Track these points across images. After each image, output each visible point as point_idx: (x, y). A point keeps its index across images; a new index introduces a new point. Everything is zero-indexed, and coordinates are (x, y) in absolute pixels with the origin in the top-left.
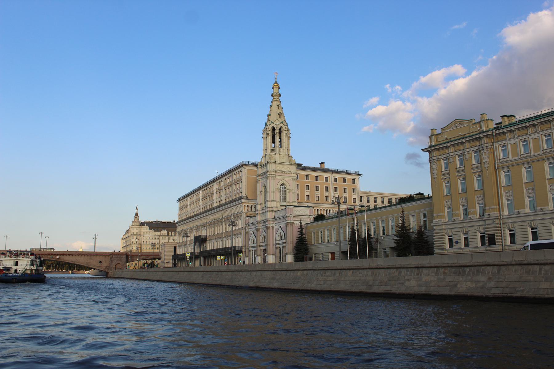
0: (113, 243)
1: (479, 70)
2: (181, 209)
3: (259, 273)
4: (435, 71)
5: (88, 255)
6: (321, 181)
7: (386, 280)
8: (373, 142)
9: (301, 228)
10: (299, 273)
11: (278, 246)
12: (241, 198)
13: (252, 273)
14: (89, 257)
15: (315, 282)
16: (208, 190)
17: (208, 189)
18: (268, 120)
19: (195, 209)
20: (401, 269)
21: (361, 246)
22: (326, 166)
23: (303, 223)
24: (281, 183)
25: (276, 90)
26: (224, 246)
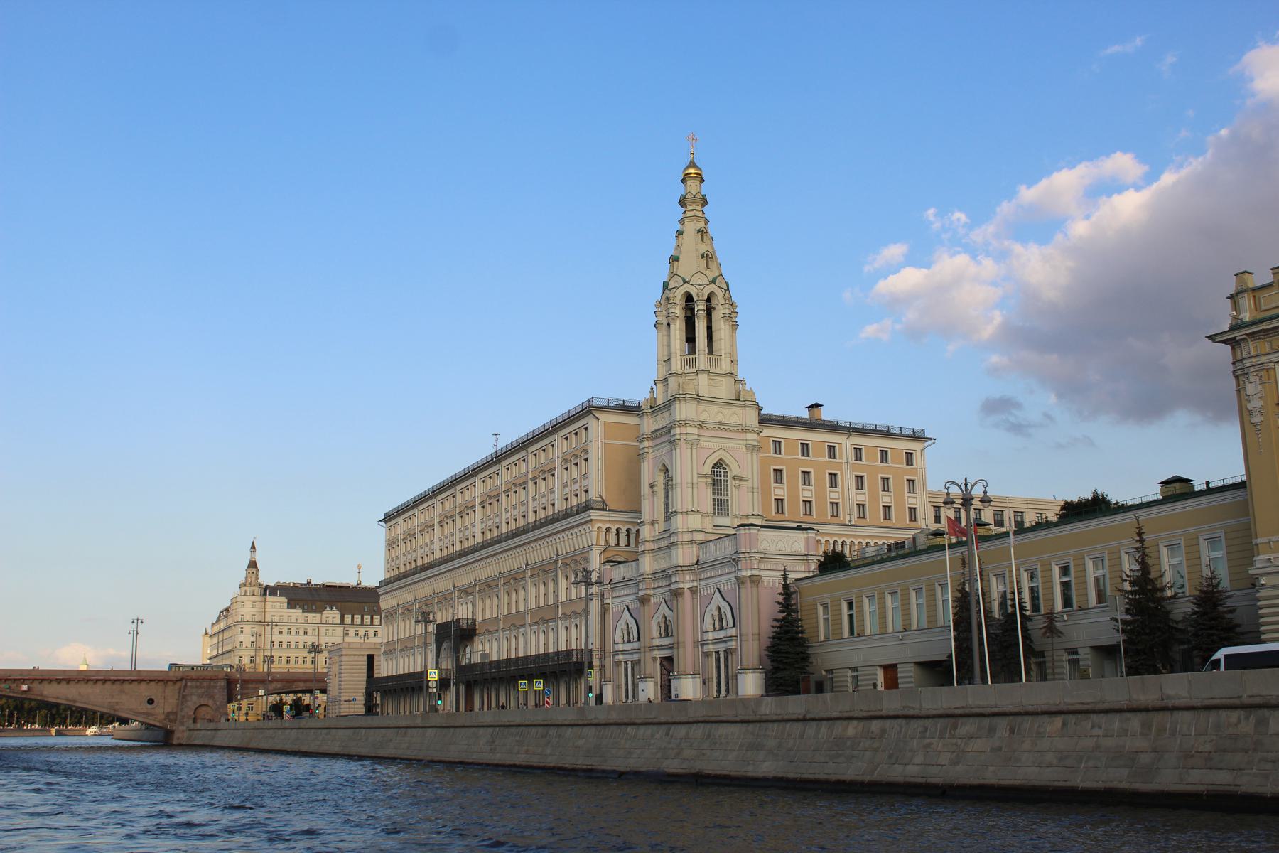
0: (189, 648)
1: (1180, 166)
2: (391, 544)
3: (698, 731)
4: (1059, 170)
5: (114, 681)
6: (818, 458)
7: (1208, 747)
8: (953, 345)
9: (787, 591)
10: (852, 729)
11: (711, 648)
12: (587, 507)
13: (673, 728)
14: (117, 686)
15: (919, 758)
16: (459, 498)
17: (458, 495)
18: (673, 275)
19: (437, 544)
20: (1266, 712)
21: (995, 644)
22: (826, 415)
23: (792, 577)
24: (713, 460)
25: (693, 186)
26: (504, 656)
